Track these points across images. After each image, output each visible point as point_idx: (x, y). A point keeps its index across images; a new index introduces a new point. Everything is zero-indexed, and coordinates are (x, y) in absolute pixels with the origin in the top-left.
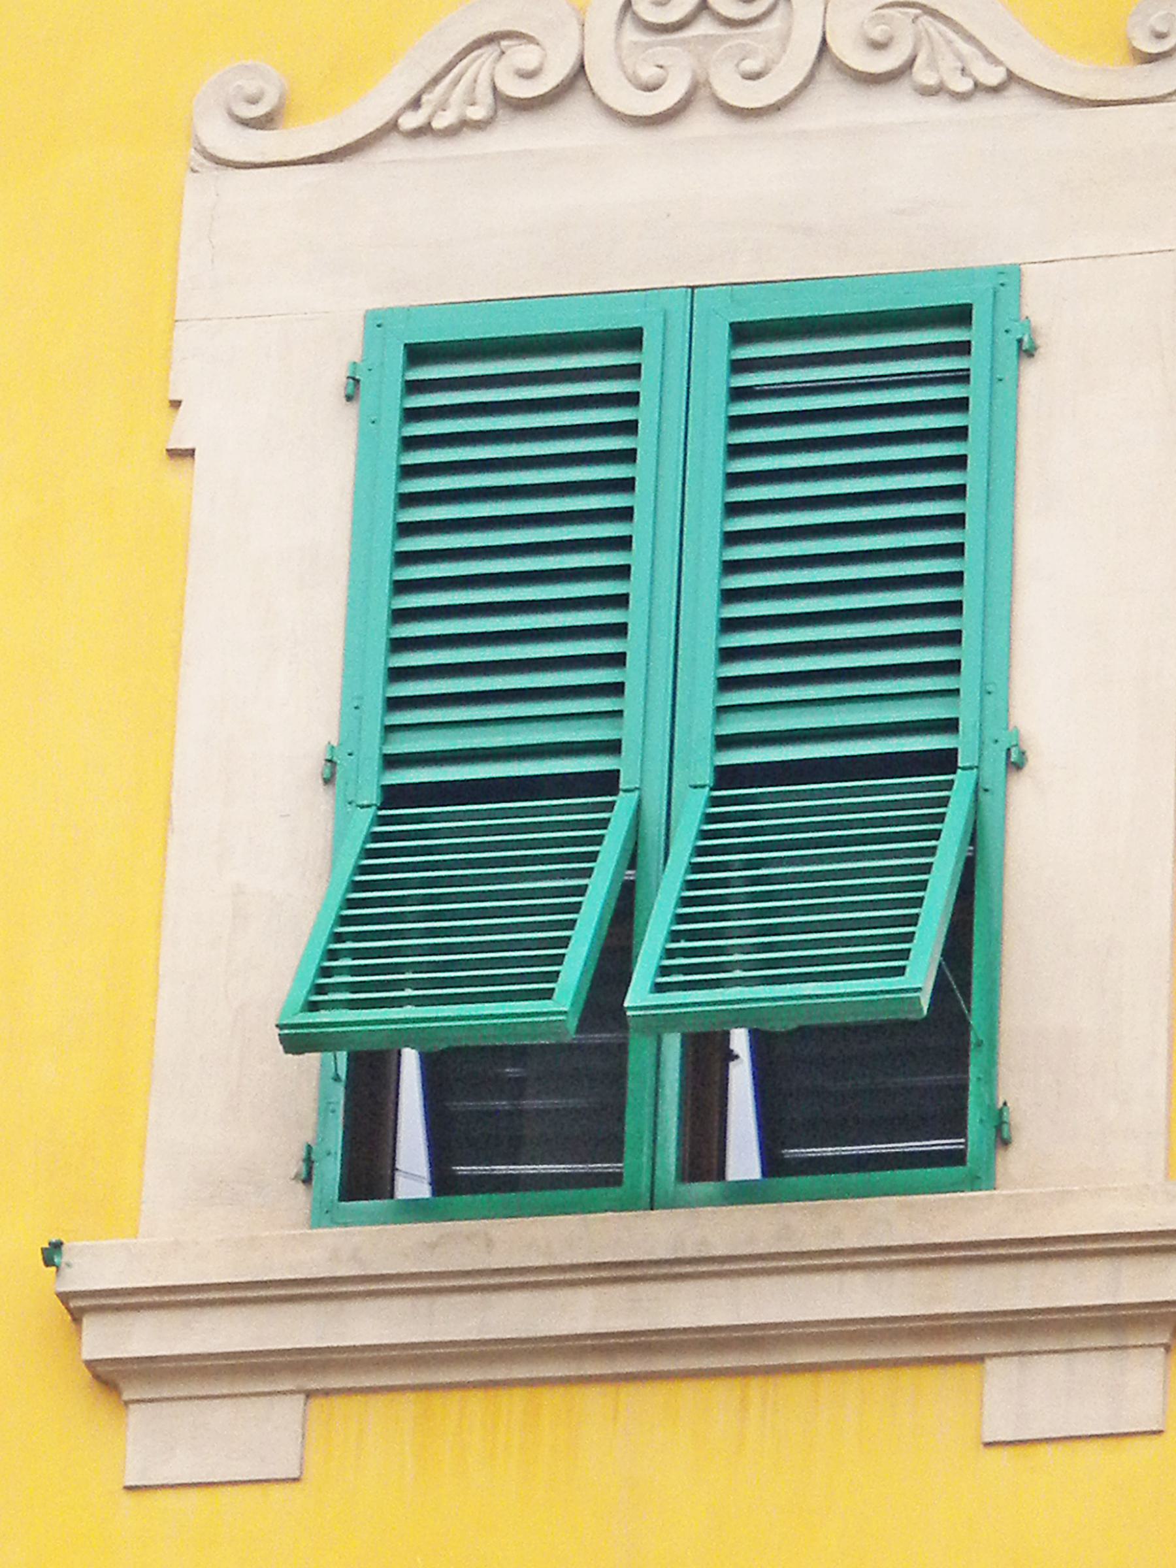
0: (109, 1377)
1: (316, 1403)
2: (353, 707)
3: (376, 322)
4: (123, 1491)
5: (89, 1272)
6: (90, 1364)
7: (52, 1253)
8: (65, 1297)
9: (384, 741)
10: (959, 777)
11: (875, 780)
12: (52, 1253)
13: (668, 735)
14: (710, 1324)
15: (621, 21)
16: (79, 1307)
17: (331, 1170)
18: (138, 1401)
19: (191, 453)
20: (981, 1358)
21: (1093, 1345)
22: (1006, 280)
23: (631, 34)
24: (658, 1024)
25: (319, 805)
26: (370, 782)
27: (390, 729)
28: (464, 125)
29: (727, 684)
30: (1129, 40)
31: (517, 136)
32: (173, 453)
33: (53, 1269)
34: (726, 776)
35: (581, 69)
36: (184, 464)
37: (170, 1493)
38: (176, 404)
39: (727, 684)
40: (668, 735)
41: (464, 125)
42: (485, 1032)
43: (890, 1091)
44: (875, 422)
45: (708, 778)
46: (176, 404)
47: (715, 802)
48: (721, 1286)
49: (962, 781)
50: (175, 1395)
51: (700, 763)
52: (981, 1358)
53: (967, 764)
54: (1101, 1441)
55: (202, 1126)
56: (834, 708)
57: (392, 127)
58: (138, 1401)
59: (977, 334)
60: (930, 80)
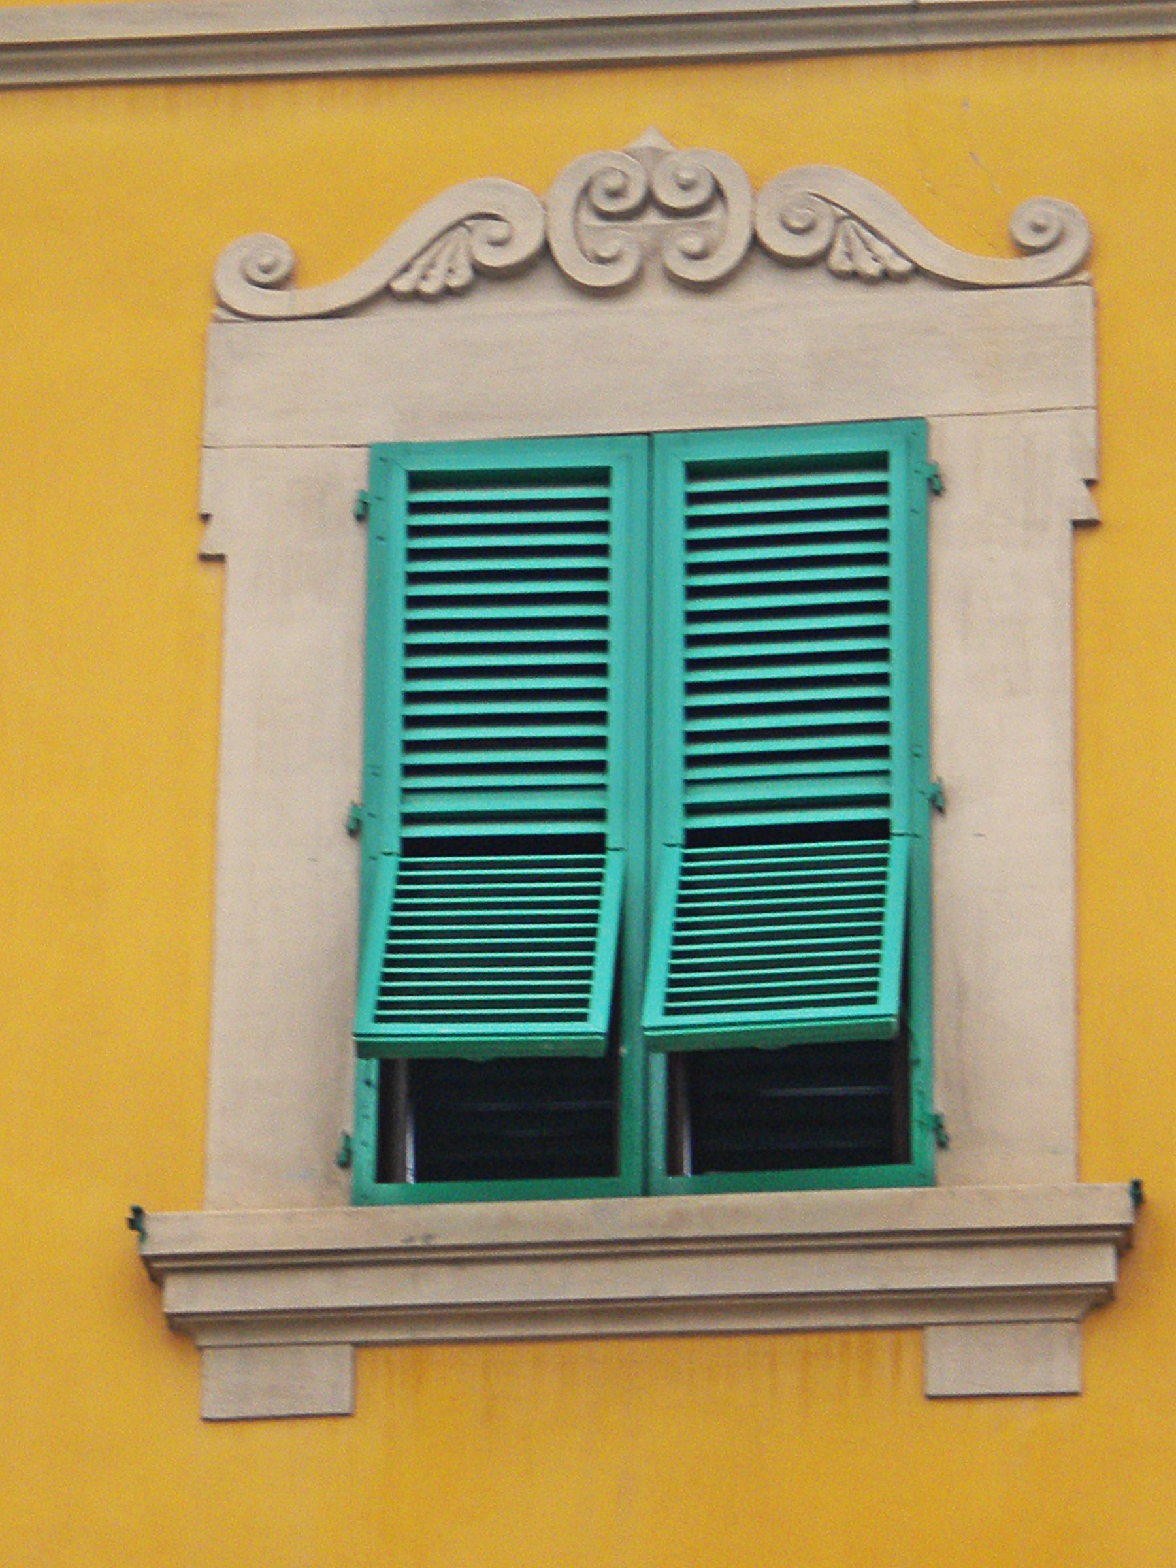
0: (184, 1328)
1: (366, 1354)
2: (372, 773)
3: (382, 456)
4: (202, 1423)
5: (166, 1237)
6: (171, 1317)
7: (136, 1220)
8: (147, 1260)
9: (403, 802)
10: (609, 857)
11: (826, 848)
12: (136, 1220)
13: (644, 803)
14: (669, 1294)
15: (577, 210)
16: (157, 1270)
17: (366, 1156)
18: (937, 1324)
19: (220, 559)
20: (920, 1327)
21: (256, 1341)
22: (915, 430)
23: (589, 219)
24: (652, 1045)
25: (343, 858)
26: (392, 834)
27: (690, 783)
28: (448, 293)
29: (693, 761)
30: (1011, 234)
31: (492, 304)
32: (205, 558)
33: (135, 1233)
34: (694, 838)
35: (546, 250)
36: (214, 568)
37: (1030, 1403)
38: (205, 518)
39: (693, 761)
40: (644, 803)
41: (448, 293)
42: (546, 1046)
43: (831, 1104)
44: (812, 546)
45: (679, 838)
46: (205, 518)
47: (404, 867)
48: (815, 1259)
49: (898, 849)
50: (943, 1320)
51: (676, 825)
52: (920, 1327)
53: (617, 846)
54: (229, 1426)
55: (262, 1119)
56: (483, 795)
57: (387, 293)
58: (937, 1324)
59: (894, 476)
60: (847, 266)
